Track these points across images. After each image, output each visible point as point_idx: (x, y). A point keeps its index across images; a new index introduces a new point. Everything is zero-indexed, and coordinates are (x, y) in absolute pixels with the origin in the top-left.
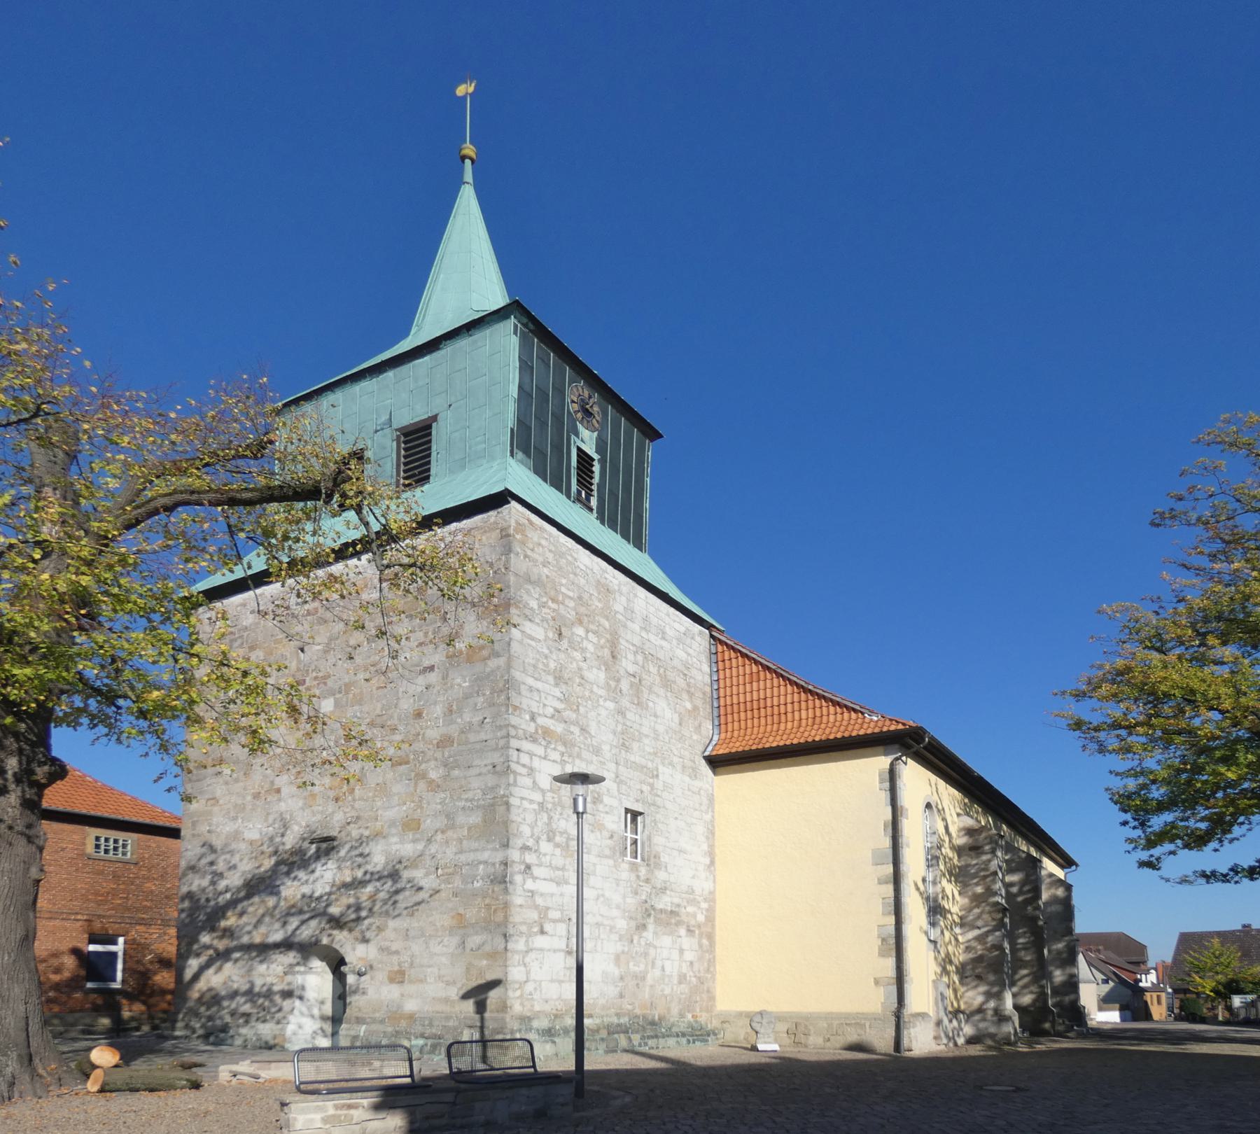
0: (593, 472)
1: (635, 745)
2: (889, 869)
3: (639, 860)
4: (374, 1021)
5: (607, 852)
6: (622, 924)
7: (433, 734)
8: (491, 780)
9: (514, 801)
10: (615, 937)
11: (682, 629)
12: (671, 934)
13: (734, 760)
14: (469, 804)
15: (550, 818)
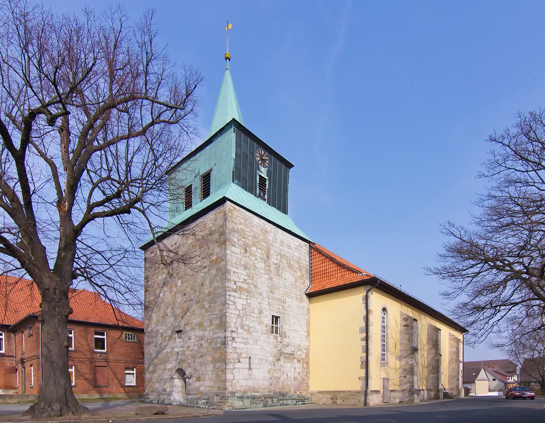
0: (266, 185)
1: (276, 291)
2: (364, 335)
5: (265, 332)
6: (271, 359)
7: (206, 291)
8: (221, 307)
9: (227, 314)
11: (298, 244)
14: (216, 316)
15: (242, 320)
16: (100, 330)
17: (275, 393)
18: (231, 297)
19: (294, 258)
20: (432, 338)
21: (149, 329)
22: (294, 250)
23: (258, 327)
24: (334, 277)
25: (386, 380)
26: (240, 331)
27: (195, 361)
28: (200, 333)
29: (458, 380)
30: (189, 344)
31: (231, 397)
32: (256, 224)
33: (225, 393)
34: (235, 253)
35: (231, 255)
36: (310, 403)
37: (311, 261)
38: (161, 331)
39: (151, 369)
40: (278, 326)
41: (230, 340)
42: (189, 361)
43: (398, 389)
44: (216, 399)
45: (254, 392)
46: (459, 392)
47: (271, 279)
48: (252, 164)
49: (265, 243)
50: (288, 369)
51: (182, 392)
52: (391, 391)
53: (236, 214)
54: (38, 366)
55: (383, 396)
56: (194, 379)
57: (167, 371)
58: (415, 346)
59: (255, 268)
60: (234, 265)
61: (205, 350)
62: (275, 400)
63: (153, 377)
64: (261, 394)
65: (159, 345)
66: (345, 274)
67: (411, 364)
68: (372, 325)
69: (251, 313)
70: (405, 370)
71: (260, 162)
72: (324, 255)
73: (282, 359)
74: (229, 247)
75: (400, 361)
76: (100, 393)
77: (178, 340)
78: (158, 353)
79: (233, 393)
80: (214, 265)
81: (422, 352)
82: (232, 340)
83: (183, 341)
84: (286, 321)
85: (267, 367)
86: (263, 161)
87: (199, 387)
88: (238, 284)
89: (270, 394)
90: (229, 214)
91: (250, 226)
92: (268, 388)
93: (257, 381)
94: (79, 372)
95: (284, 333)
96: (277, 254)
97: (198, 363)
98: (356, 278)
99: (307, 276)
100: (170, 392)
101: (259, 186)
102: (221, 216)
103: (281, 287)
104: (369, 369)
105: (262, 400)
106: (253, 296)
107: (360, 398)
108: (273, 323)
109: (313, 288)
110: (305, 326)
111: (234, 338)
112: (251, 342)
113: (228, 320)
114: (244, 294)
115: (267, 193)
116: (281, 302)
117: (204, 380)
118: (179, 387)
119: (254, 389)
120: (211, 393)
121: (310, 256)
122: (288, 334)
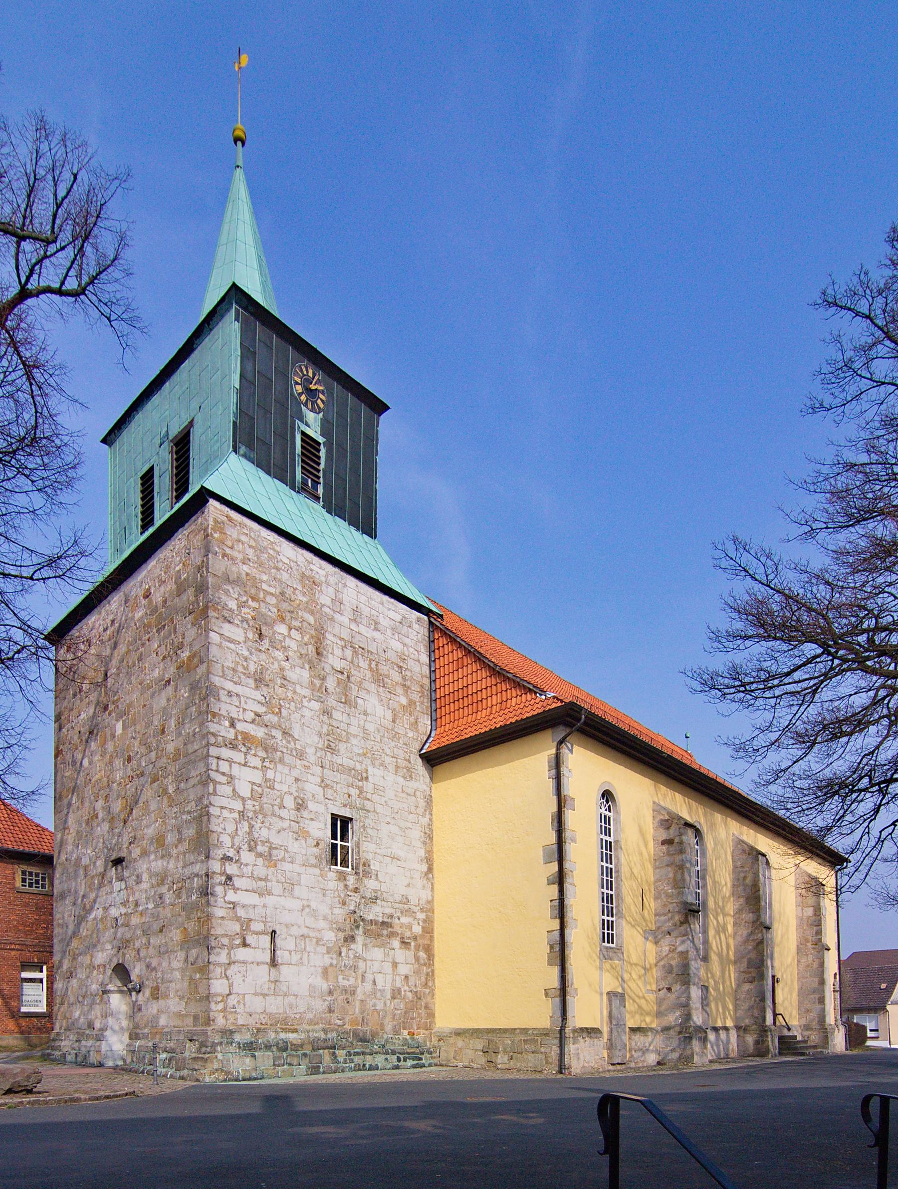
0: (319, 458)
1: (342, 747)
2: (555, 867)
5: (313, 861)
6: (330, 936)
7: (170, 748)
9: (213, 811)
11: (398, 618)
15: (251, 827)
17: (344, 1034)
18: (221, 762)
19: (390, 655)
20: (745, 878)
21: (63, 857)
22: (389, 632)
23: (295, 847)
25: (616, 998)
26: (247, 856)
28: (158, 865)
29: (822, 1000)
31: (221, 1044)
32: (287, 561)
33: (205, 1033)
34: (232, 641)
35: (220, 646)
36: (436, 1065)
37: (432, 664)
38: (85, 861)
39: (66, 965)
40: (349, 844)
41: (220, 884)
42: (138, 944)
43: (654, 1026)
44: (190, 1050)
45: (284, 1030)
46: (825, 1034)
47: (327, 712)
48: (282, 405)
49: (312, 613)
50: (376, 966)
52: (633, 1030)
53: (235, 536)
55: (611, 1046)
56: (147, 992)
57: (95, 972)
58: (691, 899)
59: (285, 682)
60: (230, 673)
61: (167, 912)
62: (341, 1054)
63: (70, 989)
64: (303, 1036)
65: (80, 900)
67: (682, 953)
68: (574, 840)
69: (276, 808)
70: (669, 970)
71: (303, 398)
72: (460, 646)
73: (360, 939)
74: (215, 624)
75: (656, 943)
77: (117, 885)
78: (80, 920)
79: (228, 1033)
80: (186, 674)
81: (720, 918)
82: (226, 883)
83: (126, 888)
84: (369, 831)
85: (321, 959)
86: (312, 394)
87: (156, 1018)
88: (240, 726)
89: (329, 1036)
90: (216, 535)
91: (270, 568)
92: (322, 1018)
93: (291, 999)
95: (364, 865)
96: (343, 643)
101: (303, 461)
102: (198, 540)
103: (355, 736)
104: (568, 965)
105: (305, 1055)
106: (281, 760)
107: (548, 1050)
108: (334, 837)
109: (440, 736)
110: (419, 844)
111: (229, 878)
112: (277, 889)
113: (213, 827)
114: (255, 755)
115: (321, 480)
116: (354, 777)
117: (167, 996)
118: (122, 1017)
119: (285, 1021)
121: (431, 652)
122: (374, 866)
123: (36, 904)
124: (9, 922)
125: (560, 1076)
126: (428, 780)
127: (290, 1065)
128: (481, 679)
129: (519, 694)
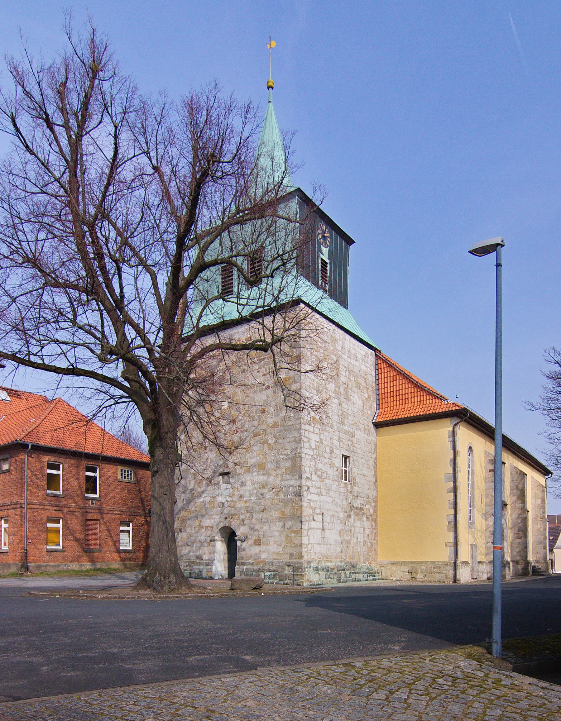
0: (327, 270)
1: (346, 421)
2: (452, 484)
3: (347, 481)
4: (249, 564)
5: (336, 478)
6: (341, 515)
7: (270, 421)
8: (294, 445)
9: (303, 456)
10: (339, 522)
11: (364, 353)
12: (360, 520)
13: (386, 424)
14: (285, 457)
15: (316, 463)
16: (92, 464)
19: (362, 373)
24: (410, 402)
27: (253, 517)
30: (241, 492)
33: (301, 563)
42: (242, 517)
51: (224, 560)
52: (480, 562)
54: (21, 519)
55: (472, 570)
56: (251, 542)
57: (203, 530)
61: (268, 502)
62: (348, 573)
66: (425, 399)
71: (322, 241)
72: (395, 369)
75: (486, 520)
76: (92, 561)
77: (223, 486)
78: (189, 502)
85: (339, 527)
94: (68, 528)
97: (257, 519)
98: (442, 408)
99: (373, 398)
100: (209, 560)
104: (458, 532)
109: (382, 414)
113: (303, 464)
118: (221, 553)
120: (279, 562)
122: (357, 480)
123: (128, 488)
124: (115, 498)
125: (454, 584)
126: (375, 435)
127: (331, 578)
128: (408, 388)
129: (431, 398)
